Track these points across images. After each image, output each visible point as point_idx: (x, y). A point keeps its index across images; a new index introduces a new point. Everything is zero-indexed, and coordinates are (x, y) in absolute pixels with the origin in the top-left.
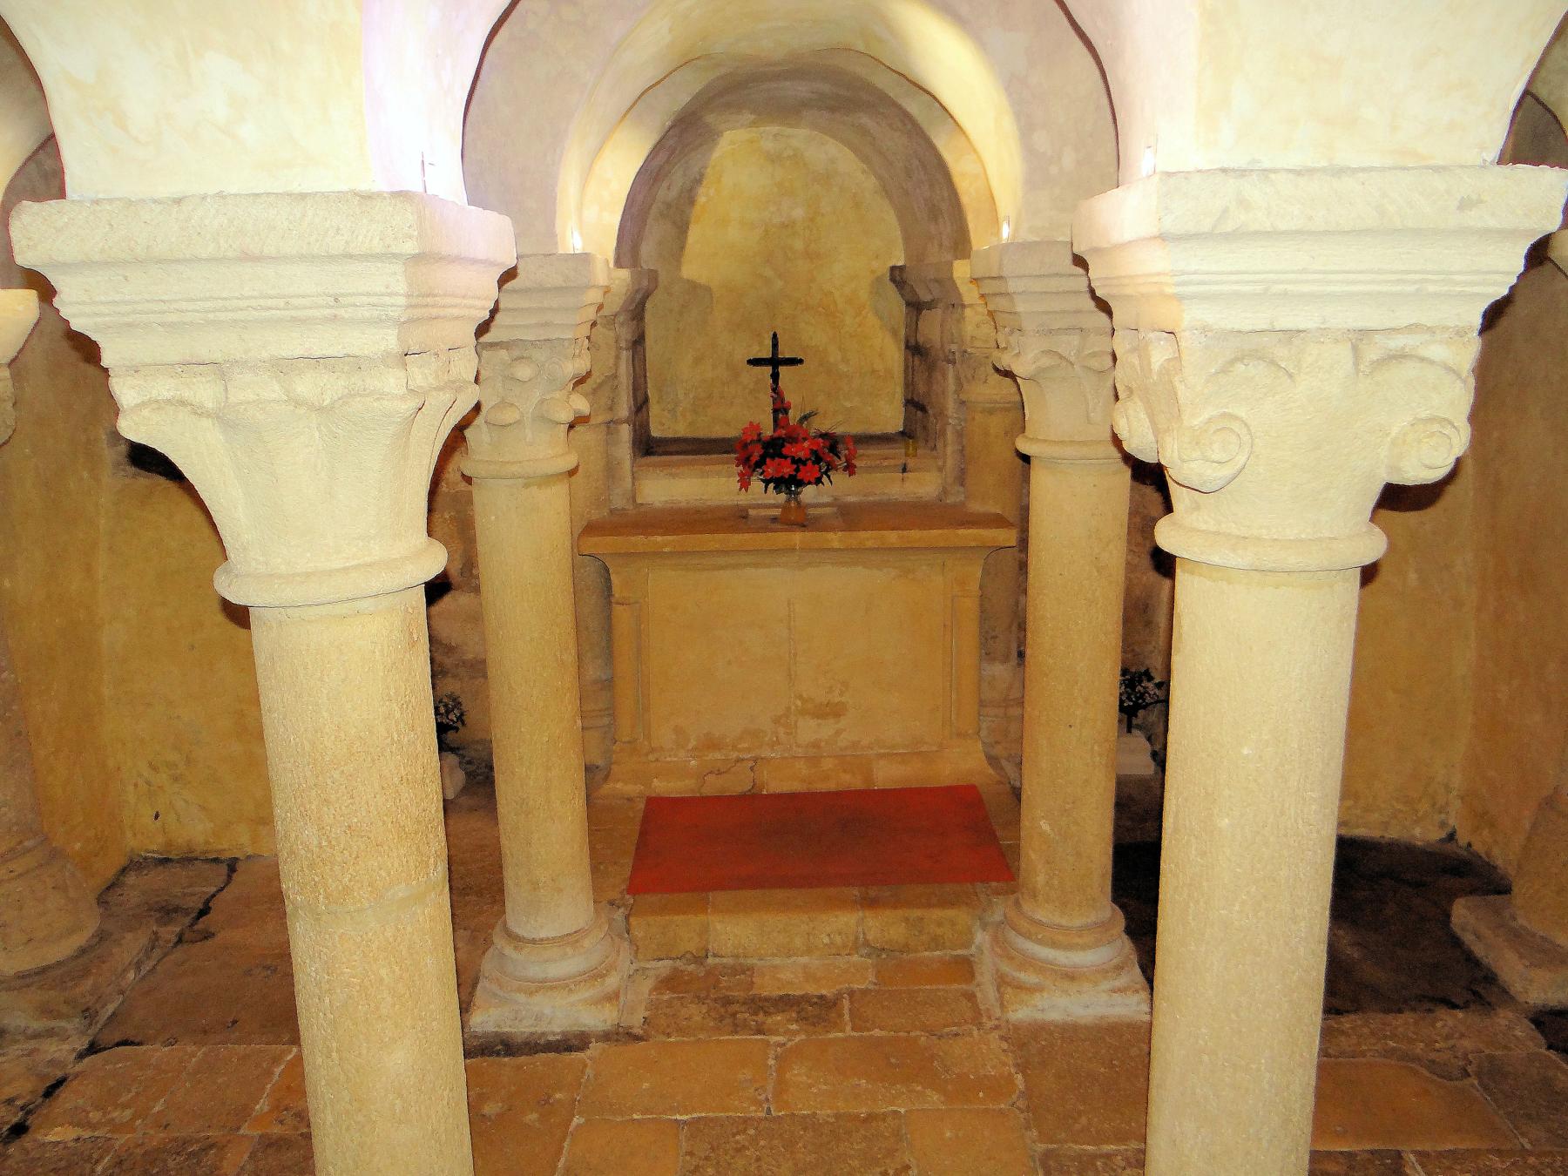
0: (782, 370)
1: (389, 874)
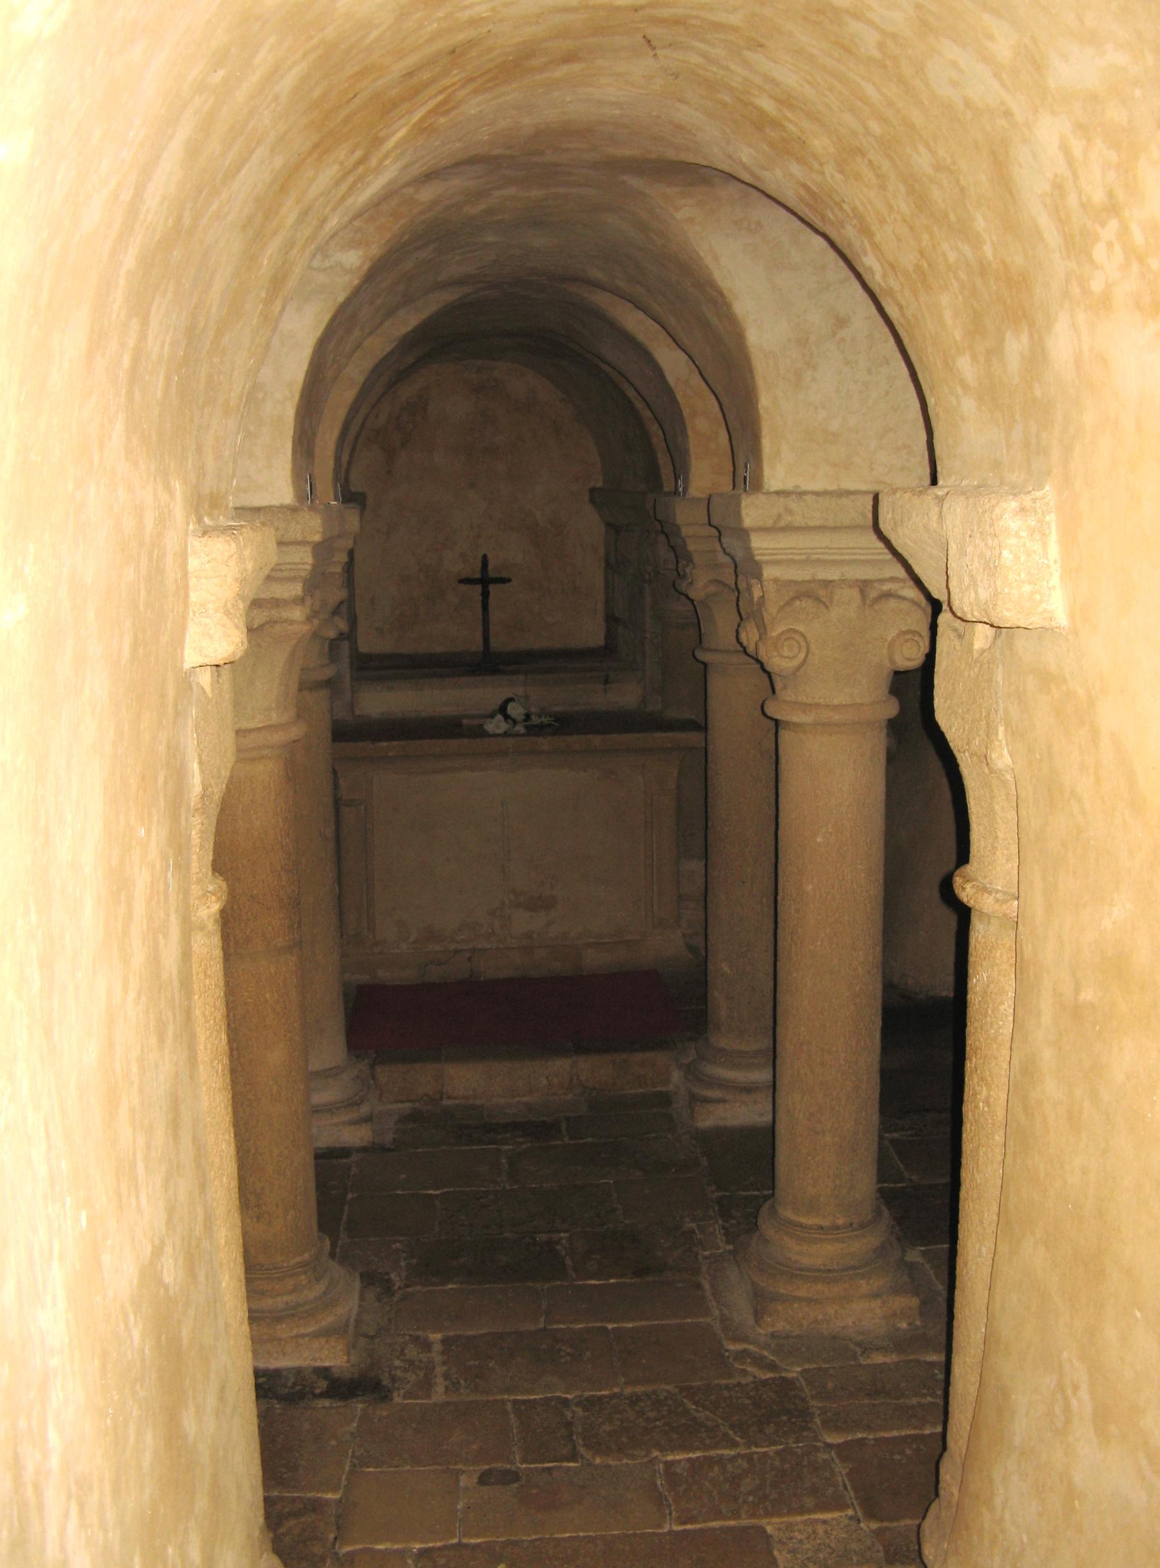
0: (492, 588)
1: (273, 929)
